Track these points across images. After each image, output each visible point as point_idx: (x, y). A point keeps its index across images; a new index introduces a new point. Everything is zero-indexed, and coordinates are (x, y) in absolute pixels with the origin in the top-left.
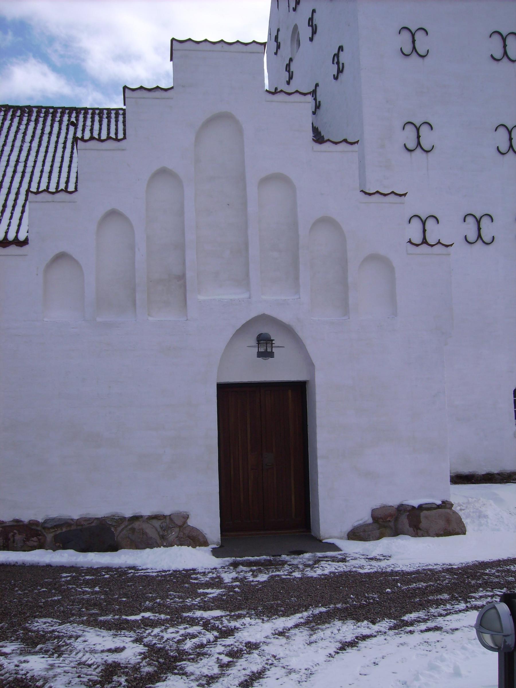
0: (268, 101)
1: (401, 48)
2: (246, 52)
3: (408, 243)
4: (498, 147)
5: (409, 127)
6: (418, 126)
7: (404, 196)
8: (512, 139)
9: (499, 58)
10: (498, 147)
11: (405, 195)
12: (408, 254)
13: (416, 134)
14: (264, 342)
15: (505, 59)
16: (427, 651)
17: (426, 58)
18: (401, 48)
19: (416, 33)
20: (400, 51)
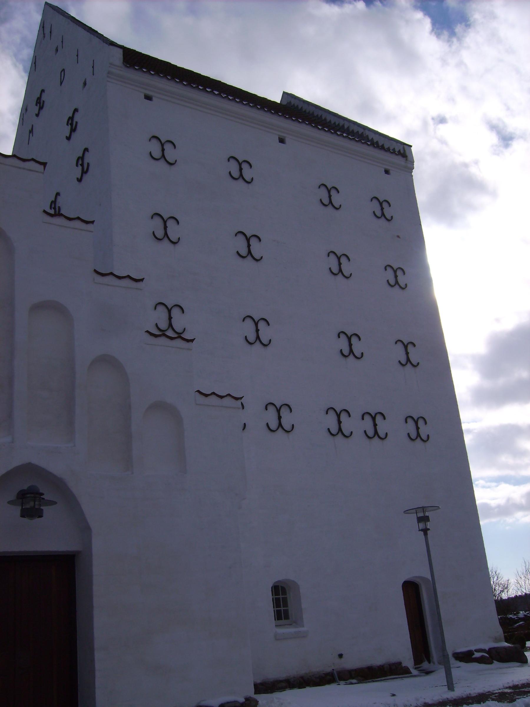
0: (45, 222)
1: (153, 232)
2: (24, 169)
3: (196, 392)
4: (246, 337)
5: (161, 308)
6: (169, 307)
7: (191, 342)
8: (259, 330)
9: (244, 256)
10: (246, 337)
11: (192, 341)
12: (197, 404)
13: (168, 315)
14: (32, 495)
15: (249, 257)
16: (382, 704)
17: (177, 245)
18: (153, 232)
19: (167, 221)
20: (152, 235)
